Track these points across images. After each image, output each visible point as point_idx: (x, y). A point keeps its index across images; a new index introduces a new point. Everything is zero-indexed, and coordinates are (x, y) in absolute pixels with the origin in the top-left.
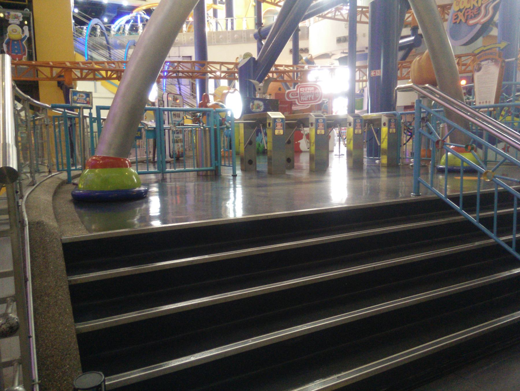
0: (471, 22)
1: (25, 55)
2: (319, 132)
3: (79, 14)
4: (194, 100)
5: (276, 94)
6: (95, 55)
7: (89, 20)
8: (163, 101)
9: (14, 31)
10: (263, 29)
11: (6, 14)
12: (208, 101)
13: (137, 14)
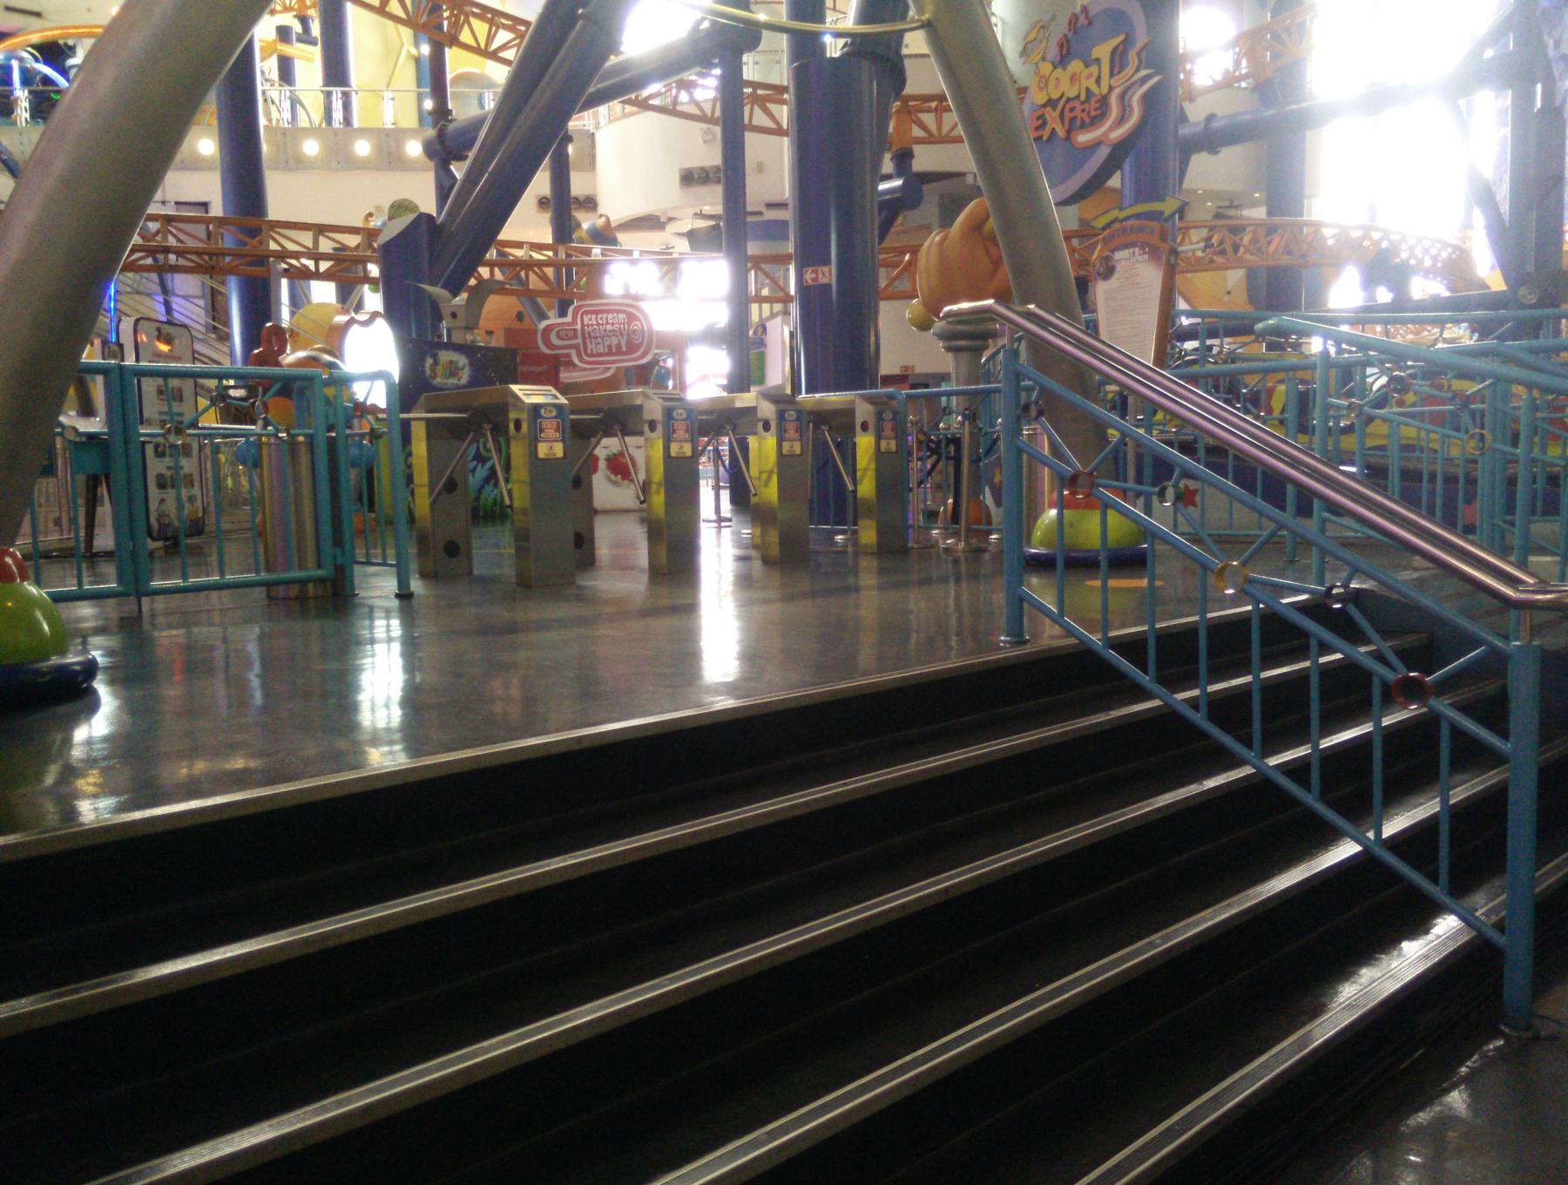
0: (1083, 138)
2: (674, 449)
4: (220, 346)
5: (509, 332)
8: (121, 346)
10: (451, 127)
13: (9, 59)
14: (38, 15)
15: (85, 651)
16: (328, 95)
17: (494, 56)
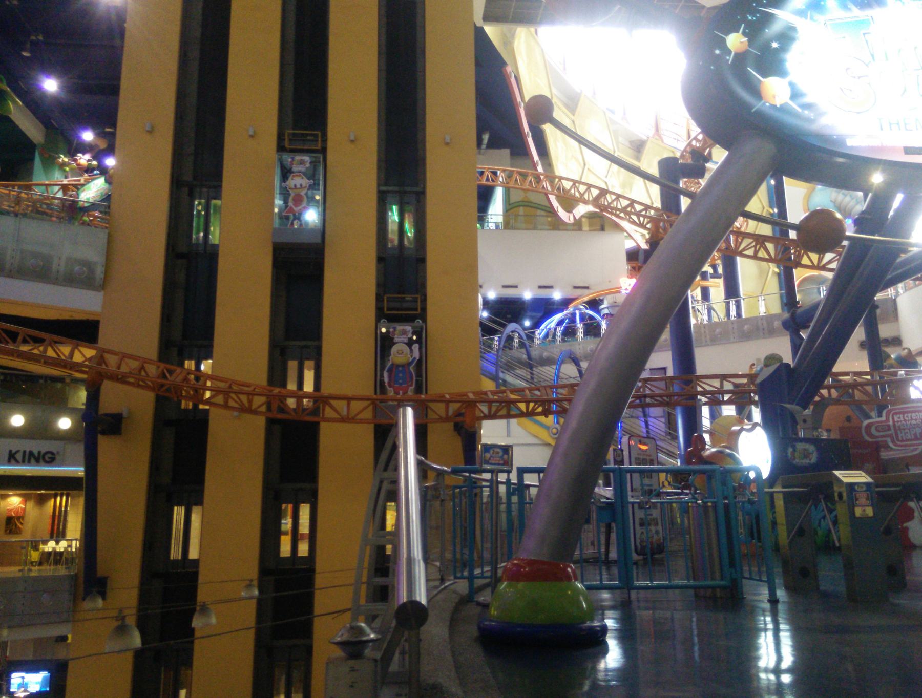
1: (411, 385)
3: (489, 319)
5: (842, 429)
6: (509, 378)
7: (504, 326)
9: (400, 352)
10: (799, 311)
11: (391, 330)
12: (704, 448)
13: (574, 310)
14: (587, 288)
15: (603, 619)
16: (728, 304)
17: (823, 268)
